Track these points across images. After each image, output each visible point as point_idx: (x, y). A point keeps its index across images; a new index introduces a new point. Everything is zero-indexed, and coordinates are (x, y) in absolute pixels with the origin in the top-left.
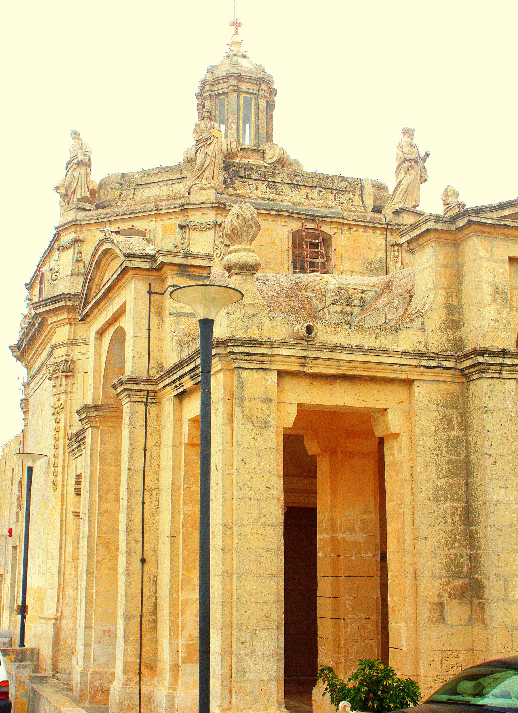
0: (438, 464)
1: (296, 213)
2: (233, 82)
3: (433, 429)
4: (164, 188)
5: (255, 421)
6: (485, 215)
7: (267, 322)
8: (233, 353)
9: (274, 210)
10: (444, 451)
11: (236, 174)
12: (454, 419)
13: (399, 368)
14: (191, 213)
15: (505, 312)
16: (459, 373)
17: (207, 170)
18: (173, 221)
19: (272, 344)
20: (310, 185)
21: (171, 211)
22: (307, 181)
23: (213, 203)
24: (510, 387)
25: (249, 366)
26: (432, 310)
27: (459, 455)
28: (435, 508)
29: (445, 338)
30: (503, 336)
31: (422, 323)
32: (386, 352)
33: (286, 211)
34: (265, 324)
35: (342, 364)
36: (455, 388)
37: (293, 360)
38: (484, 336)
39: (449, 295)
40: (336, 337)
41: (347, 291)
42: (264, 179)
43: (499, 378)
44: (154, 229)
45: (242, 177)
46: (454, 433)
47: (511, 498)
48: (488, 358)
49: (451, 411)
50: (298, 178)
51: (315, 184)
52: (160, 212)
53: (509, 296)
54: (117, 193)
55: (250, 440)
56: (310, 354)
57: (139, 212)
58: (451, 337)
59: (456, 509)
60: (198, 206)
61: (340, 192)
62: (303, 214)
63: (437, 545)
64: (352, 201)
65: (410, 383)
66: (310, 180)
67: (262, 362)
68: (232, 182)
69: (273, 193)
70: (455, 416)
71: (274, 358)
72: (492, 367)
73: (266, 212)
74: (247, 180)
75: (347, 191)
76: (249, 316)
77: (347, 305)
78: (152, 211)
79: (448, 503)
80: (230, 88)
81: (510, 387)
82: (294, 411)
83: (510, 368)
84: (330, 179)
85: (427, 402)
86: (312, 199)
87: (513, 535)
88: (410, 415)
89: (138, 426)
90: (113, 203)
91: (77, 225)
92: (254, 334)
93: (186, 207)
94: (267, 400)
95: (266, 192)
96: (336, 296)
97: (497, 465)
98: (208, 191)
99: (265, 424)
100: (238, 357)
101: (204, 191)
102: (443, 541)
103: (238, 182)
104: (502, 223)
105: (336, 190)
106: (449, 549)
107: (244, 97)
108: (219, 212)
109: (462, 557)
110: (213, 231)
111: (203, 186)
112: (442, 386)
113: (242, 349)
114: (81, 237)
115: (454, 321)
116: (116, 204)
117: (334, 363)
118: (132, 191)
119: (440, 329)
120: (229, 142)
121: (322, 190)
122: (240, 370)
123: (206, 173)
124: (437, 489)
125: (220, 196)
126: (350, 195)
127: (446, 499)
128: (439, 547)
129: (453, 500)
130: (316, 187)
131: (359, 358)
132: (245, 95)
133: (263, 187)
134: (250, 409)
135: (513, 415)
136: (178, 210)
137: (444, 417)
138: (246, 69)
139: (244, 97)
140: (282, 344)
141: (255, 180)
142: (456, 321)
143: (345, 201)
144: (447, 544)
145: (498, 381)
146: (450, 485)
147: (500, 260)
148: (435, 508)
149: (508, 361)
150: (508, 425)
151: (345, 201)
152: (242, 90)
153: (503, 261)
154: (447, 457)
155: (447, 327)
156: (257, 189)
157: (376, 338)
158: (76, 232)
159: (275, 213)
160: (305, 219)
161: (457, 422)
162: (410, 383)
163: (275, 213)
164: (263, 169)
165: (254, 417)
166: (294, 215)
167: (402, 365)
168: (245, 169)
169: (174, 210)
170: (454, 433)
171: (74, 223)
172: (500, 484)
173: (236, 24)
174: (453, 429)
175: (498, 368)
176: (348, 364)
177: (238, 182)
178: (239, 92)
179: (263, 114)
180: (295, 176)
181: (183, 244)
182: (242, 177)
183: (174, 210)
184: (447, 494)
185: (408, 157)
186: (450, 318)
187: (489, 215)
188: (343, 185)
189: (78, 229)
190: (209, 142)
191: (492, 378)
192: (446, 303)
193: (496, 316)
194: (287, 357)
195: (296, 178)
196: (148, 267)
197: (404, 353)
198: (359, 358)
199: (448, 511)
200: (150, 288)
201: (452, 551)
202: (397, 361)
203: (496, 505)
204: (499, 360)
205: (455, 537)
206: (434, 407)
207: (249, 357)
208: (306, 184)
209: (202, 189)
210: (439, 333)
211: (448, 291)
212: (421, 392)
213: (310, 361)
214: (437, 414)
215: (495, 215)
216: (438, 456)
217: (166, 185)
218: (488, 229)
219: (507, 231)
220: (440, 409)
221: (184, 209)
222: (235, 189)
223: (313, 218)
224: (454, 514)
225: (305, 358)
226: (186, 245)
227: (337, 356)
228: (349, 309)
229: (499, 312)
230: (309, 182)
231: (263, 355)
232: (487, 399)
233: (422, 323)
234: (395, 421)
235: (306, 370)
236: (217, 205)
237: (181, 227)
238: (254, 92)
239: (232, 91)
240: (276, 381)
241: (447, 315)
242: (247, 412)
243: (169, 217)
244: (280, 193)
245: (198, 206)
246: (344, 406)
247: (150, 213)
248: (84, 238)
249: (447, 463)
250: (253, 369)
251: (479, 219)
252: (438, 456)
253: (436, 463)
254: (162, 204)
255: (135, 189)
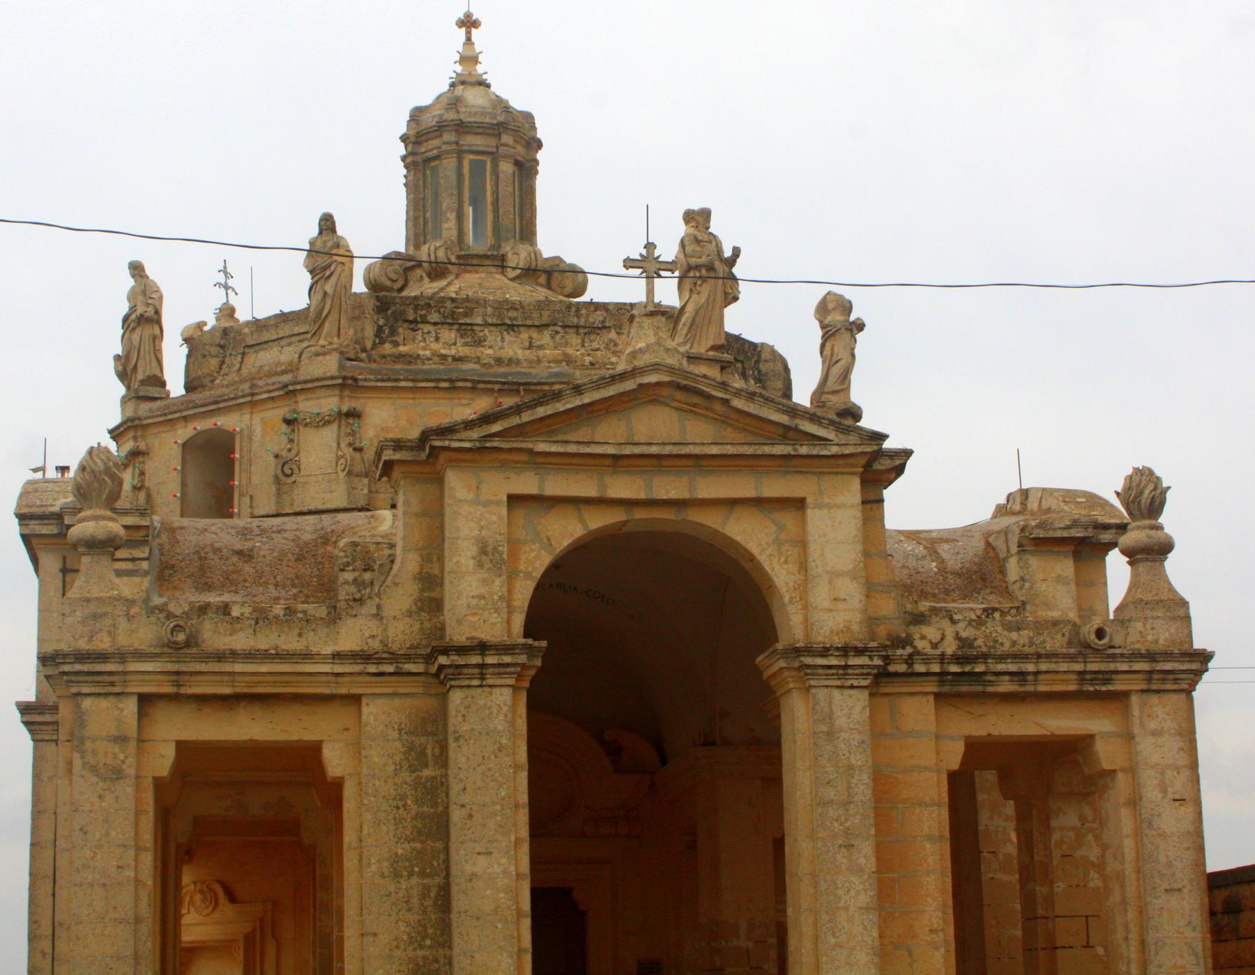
0: (398, 822)
1: (484, 382)
2: (448, 137)
3: (392, 768)
4: (287, 349)
5: (102, 770)
6: (458, 436)
7: (123, 624)
8: (64, 673)
9: (445, 380)
10: (409, 802)
11: (399, 317)
12: (429, 751)
13: (333, 679)
14: (301, 398)
15: (498, 582)
16: (434, 680)
17: (330, 318)
18: (276, 412)
19: (122, 657)
20: (536, 323)
21: (272, 395)
22: (530, 318)
23: (333, 378)
24: (502, 699)
25: (93, 690)
26: (396, 584)
27: (435, 805)
28: (392, 888)
29: (417, 626)
30: (492, 620)
31: (379, 607)
32: (307, 656)
33: (466, 380)
34: (121, 627)
35: (238, 678)
36: (431, 703)
37: (159, 677)
38: (459, 622)
39: (426, 559)
40: (234, 637)
41: (366, 547)
42: (451, 320)
43: (481, 686)
44: (250, 428)
45: (411, 322)
46: (427, 773)
47: (497, 869)
48: (456, 657)
49: (423, 739)
50: (512, 314)
51: (545, 320)
52: (257, 398)
53: (505, 556)
54: (214, 362)
55: (95, 799)
56: (184, 668)
57: (225, 401)
58: (427, 625)
59: (427, 888)
60: (309, 385)
61: (593, 330)
62: (497, 383)
63: (394, 943)
64: (616, 345)
65: (356, 699)
66: (535, 315)
67: (112, 684)
68: (393, 332)
69: (466, 344)
70: (430, 747)
71: (128, 678)
72: (465, 671)
73: (430, 384)
74: (420, 326)
75: (605, 327)
76: (95, 617)
77: (365, 570)
78: (244, 396)
79: (415, 880)
80: (444, 148)
81: (502, 699)
82: (170, 752)
83: (496, 670)
84: (573, 309)
85: (382, 727)
86: (541, 347)
87: (500, 926)
88: (357, 749)
89: (45, 779)
90: (206, 381)
91: (136, 427)
92: (103, 643)
93: (291, 388)
94: (121, 739)
95: (455, 344)
96: (346, 556)
97: (474, 819)
98: (328, 357)
99: (117, 774)
100: (73, 678)
101: (320, 358)
102: (405, 937)
103: (402, 331)
104: (488, 445)
105: (585, 327)
106: (414, 950)
107: (471, 162)
108: (347, 393)
109: (437, 961)
110: (335, 426)
111: (321, 350)
112: (408, 702)
113: (78, 667)
114: (142, 446)
115: (431, 600)
116: (212, 381)
117: (226, 678)
118: (239, 358)
119: (410, 614)
120: (432, 248)
121: (559, 329)
122: (79, 698)
123: (327, 325)
124: (396, 859)
125: (349, 363)
126: (613, 335)
127: (411, 874)
128: (397, 947)
129: (422, 874)
130: (547, 326)
131: (264, 668)
132: (472, 157)
133: (448, 335)
134: (94, 753)
135: (504, 741)
136: (282, 393)
137: (411, 749)
138: (473, 110)
139: (471, 162)
140: (140, 655)
141: (435, 324)
142: (436, 600)
143: (602, 347)
144: (411, 943)
145: (479, 690)
146: (419, 852)
147: (491, 502)
148: (392, 888)
149: (490, 660)
150: (496, 757)
151: (602, 347)
152: (466, 148)
153: (498, 503)
154: (415, 809)
155: (421, 609)
156: (437, 339)
157: (300, 635)
158: (135, 438)
159: (445, 385)
160: (500, 390)
161: (433, 755)
162: (356, 699)
163: (445, 385)
164: (448, 304)
165: (101, 765)
166: (481, 386)
167: (337, 675)
168: (416, 308)
169: (276, 394)
170: (427, 773)
171: (130, 424)
172: (478, 849)
173: (468, 23)
174: (427, 766)
175: (477, 671)
176: (247, 678)
177: (402, 331)
178: (460, 154)
179: (506, 189)
180: (508, 310)
181: (290, 450)
182: (411, 322)
183: (276, 394)
184: (413, 866)
185: (693, 261)
186: (426, 594)
187: (464, 435)
188: (598, 317)
189: (139, 433)
190: (328, 273)
191: (469, 687)
192: (420, 573)
193: (483, 591)
194: (150, 674)
195: (510, 314)
196: (55, 532)
197: (337, 656)
198: (264, 668)
199: (415, 892)
200: (64, 563)
201: (420, 953)
202: (327, 668)
203: (471, 880)
204: (476, 660)
205: (426, 930)
206: (396, 735)
207: (90, 678)
208: (529, 322)
209: (317, 354)
210: (407, 620)
211: (425, 553)
212: (371, 711)
213: (186, 678)
214: (399, 744)
215: (475, 434)
216: (398, 808)
217: (290, 344)
218: (468, 456)
219: (502, 456)
220: (405, 737)
221: (289, 392)
222: (396, 344)
223: (515, 387)
224: (424, 896)
225: (178, 673)
226: (294, 452)
227: (228, 667)
228: (367, 576)
229: (485, 582)
230: (533, 319)
231: (110, 673)
232: (460, 719)
233: (379, 607)
234: (335, 761)
235: (183, 691)
236: (340, 381)
237: (288, 422)
238: (488, 149)
239: (448, 152)
240: (135, 710)
241: (422, 590)
242: (89, 758)
243: (271, 405)
244: (479, 343)
245: (309, 385)
246: (251, 740)
247: (241, 400)
248: (148, 448)
249: (415, 818)
250: (99, 694)
251: (446, 443)
252: (398, 808)
253: (395, 819)
254: (261, 383)
255: (243, 354)
